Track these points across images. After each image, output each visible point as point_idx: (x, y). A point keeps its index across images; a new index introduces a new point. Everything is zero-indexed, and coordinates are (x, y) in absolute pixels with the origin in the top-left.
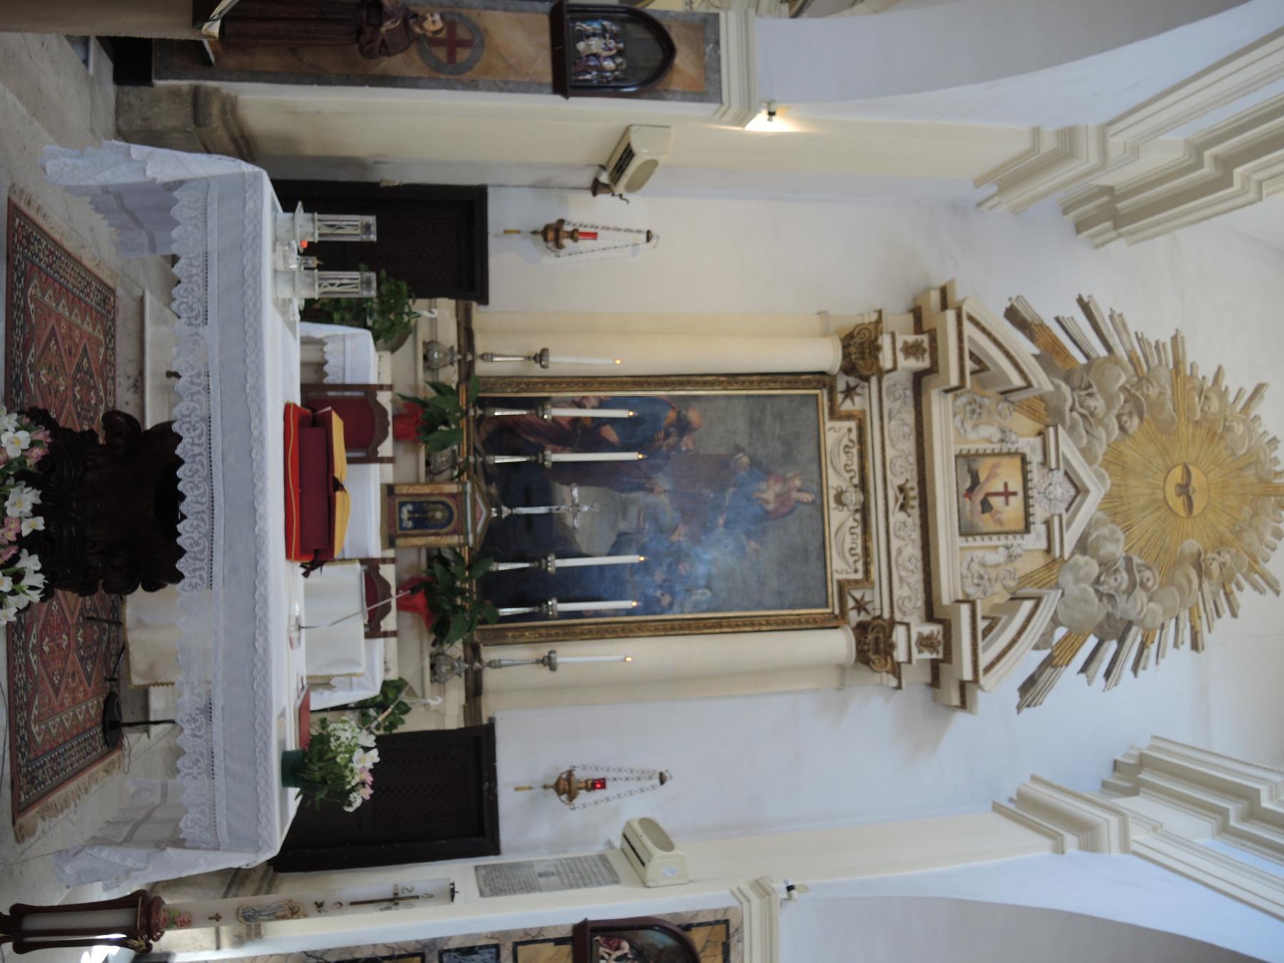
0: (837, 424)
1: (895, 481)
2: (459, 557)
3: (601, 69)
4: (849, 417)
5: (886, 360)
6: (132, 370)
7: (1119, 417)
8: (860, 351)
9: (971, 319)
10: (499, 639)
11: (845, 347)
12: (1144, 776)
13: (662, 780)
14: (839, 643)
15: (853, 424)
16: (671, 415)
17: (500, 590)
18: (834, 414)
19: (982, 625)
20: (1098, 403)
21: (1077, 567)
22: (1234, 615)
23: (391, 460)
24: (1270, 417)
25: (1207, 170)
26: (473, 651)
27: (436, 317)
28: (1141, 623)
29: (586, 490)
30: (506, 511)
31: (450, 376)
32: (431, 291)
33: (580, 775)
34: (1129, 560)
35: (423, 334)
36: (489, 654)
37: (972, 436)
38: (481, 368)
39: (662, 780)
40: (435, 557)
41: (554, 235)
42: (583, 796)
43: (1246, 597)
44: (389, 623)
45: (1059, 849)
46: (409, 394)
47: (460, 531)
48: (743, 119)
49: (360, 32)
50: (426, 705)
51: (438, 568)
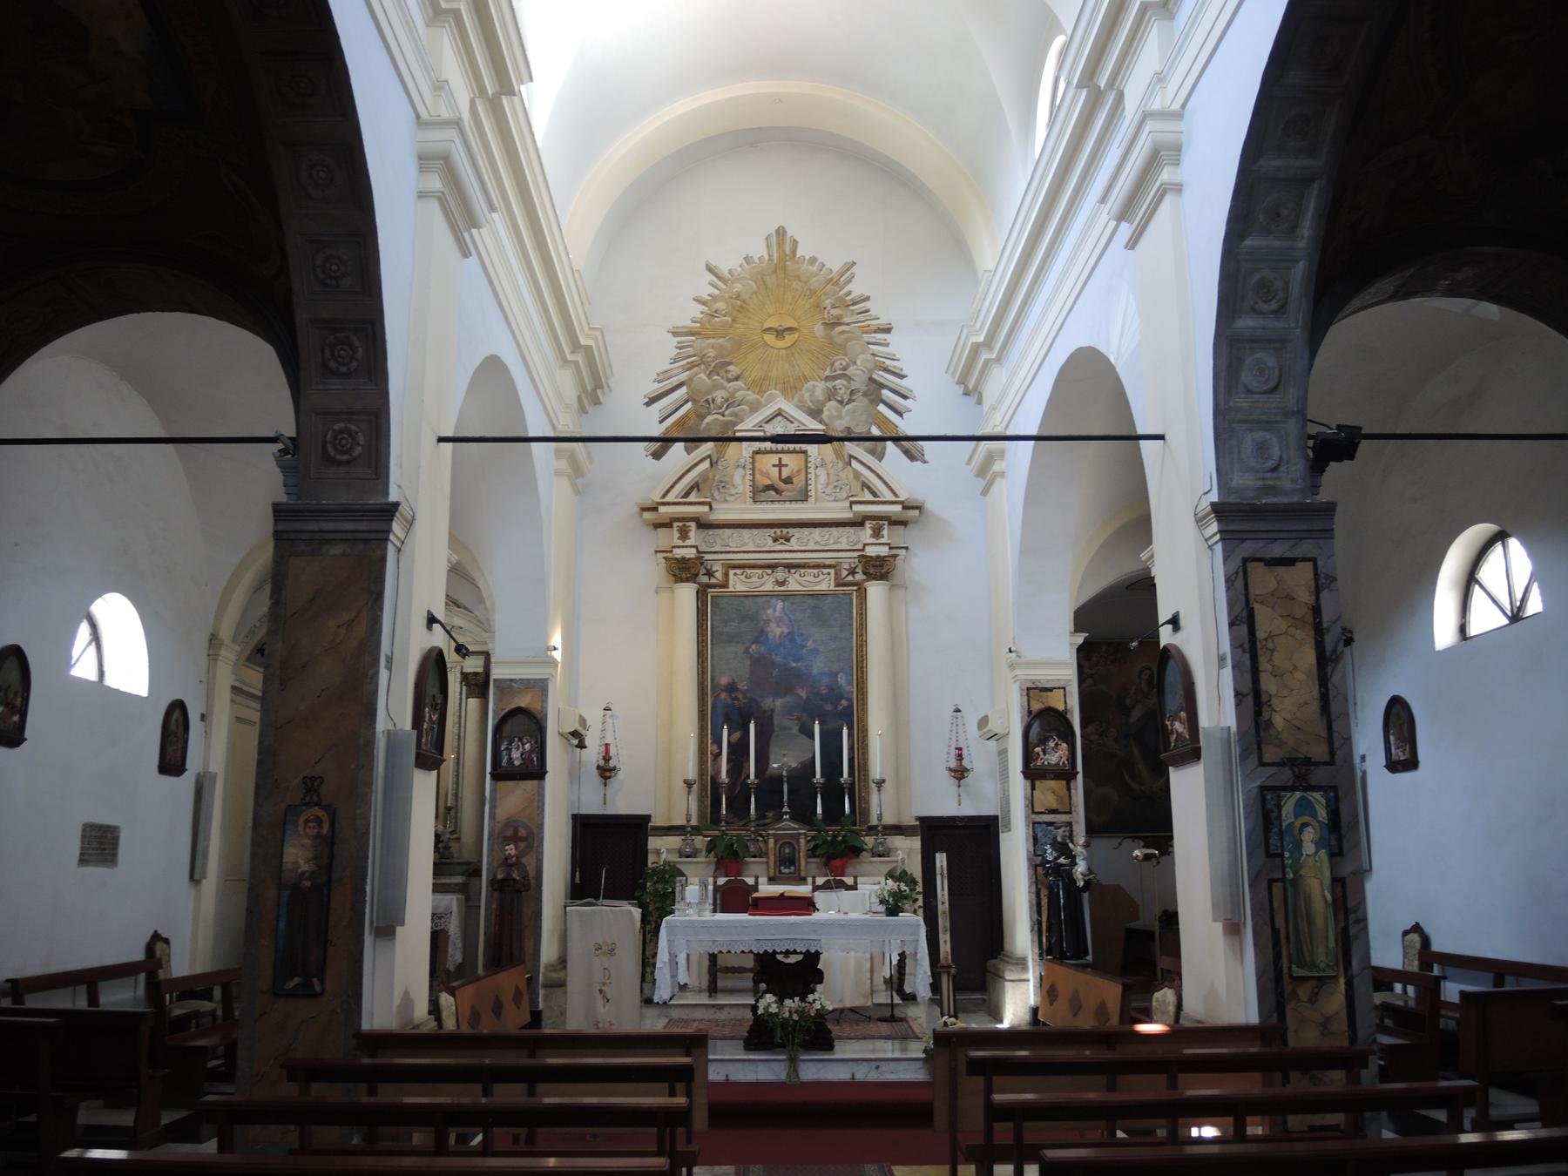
0: (731, 583)
1: (770, 545)
2: (813, 838)
3: (531, 752)
4: (726, 575)
5: (690, 553)
6: (712, 1011)
7: (730, 381)
8: (683, 570)
9: (664, 496)
10: (866, 813)
11: (682, 581)
12: (971, 386)
13: (958, 711)
14: (875, 590)
15: (731, 572)
16: (723, 696)
17: (834, 812)
18: (725, 586)
19: (868, 496)
20: (719, 395)
21: (830, 418)
22: (868, 298)
23: (757, 878)
24: (729, 262)
25: (579, 358)
26: (872, 830)
27: (662, 848)
28: (871, 371)
29: (772, 756)
30: (786, 809)
31: (700, 842)
32: (643, 850)
33: (953, 764)
34: (827, 379)
35: (674, 858)
36: (874, 821)
37: (740, 489)
38: (694, 822)
39: (958, 711)
40: (812, 853)
41: (606, 772)
42: (965, 763)
43: (856, 289)
44: (849, 881)
45: (1002, 474)
46: (713, 867)
47: (797, 837)
48: (554, 663)
49: (519, 891)
50: (903, 860)
51: (819, 851)
